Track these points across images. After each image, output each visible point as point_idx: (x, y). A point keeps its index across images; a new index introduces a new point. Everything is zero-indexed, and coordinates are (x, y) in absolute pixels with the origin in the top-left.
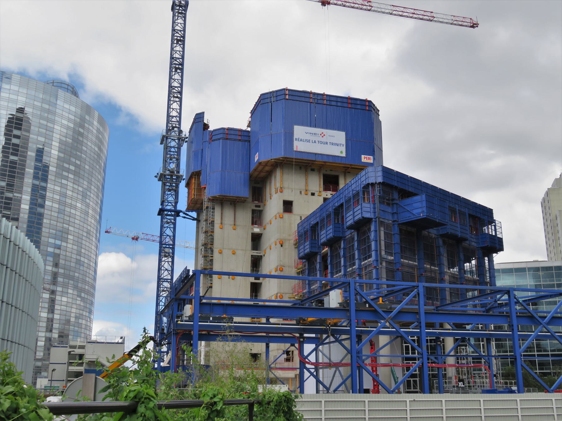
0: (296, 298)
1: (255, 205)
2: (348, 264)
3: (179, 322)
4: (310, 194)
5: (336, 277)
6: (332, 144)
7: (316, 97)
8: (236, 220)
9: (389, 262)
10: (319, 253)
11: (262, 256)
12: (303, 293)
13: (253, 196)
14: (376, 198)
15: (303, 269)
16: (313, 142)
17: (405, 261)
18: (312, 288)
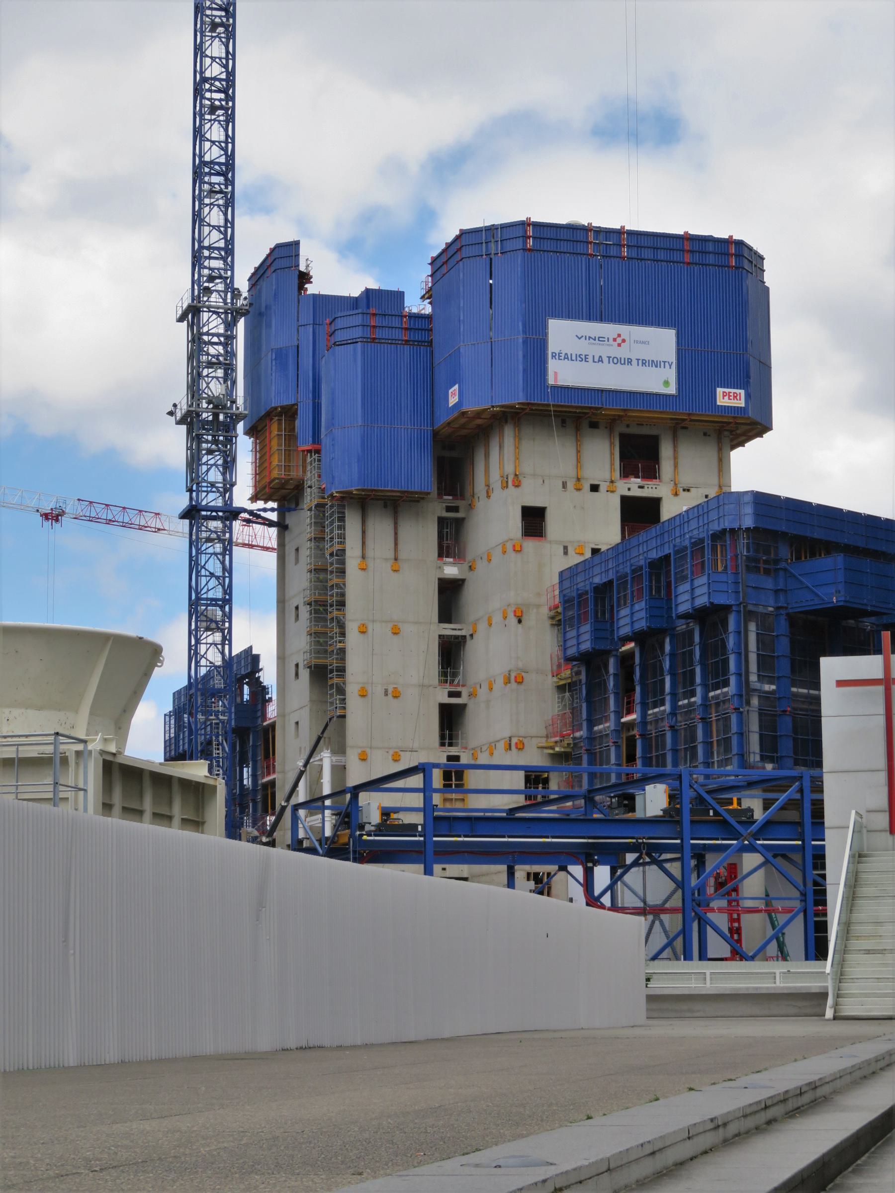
0: (557, 749)
1: (444, 505)
2: (681, 691)
3: (365, 837)
4: (587, 487)
5: (654, 713)
6: (644, 363)
7: (601, 239)
8: (400, 547)
9: (765, 697)
10: (614, 653)
11: (465, 637)
12: (574, 738)
13: (439, 482)
14: (740, 561)
15: (574, 680)
16: (596, 359)
17: (801, 690)
18: (596, 728)
